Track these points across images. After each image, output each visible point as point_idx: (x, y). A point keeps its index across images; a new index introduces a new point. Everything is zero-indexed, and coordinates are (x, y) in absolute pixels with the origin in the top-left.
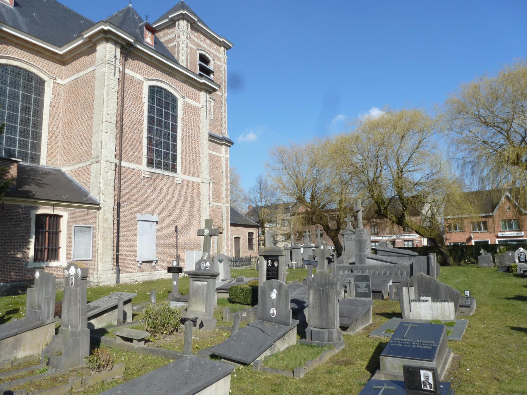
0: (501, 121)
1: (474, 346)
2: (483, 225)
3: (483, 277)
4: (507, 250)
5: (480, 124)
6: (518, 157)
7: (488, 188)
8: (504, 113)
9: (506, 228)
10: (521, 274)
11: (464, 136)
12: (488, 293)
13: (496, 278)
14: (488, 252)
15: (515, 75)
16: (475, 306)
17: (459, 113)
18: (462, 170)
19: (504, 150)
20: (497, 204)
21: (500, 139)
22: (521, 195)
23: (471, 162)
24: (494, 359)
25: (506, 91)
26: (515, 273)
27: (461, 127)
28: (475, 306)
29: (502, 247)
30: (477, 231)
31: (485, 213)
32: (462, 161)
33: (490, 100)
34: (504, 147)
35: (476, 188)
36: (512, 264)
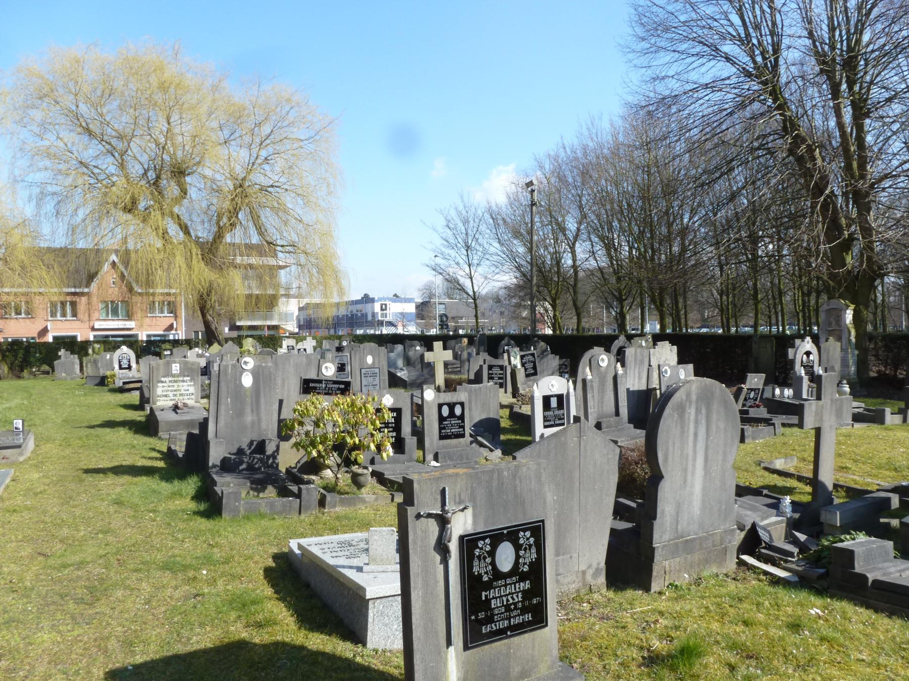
0: (114, 133)
1: (14, 511)
2: (69, 306)
3: (59, 396)
4: (105, 351)
5: (79, 130)
6: (134, 202)
7: (81, 245)
8: (121, 122)
9: (108, 314)
10: (120, 388)
11: (47, 143)
12: (59, 421)
13: (79, 396)
14: (73, 353)
15: (143, 64)
16: (31, 444)
17: (40, 98)
18: (39, 206)
19: (114, 184)
20: (97, 273)
21: (109, 165)
22: (132, 262)
23: (54, 194)
24: (46, 523)
25: (126, 85)
26: (111, 386)
27: (42, 125)
28: (31, 444)
29: (97, 346)
30: (59, 318)
31: (75, 287)
32: (38, 190)
33: (99, 93)
34: (115, 179)
35: (60, 242)
36: (108, 373)
